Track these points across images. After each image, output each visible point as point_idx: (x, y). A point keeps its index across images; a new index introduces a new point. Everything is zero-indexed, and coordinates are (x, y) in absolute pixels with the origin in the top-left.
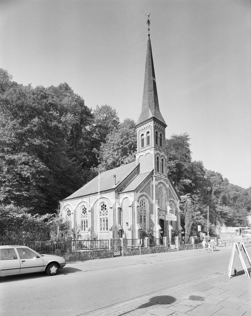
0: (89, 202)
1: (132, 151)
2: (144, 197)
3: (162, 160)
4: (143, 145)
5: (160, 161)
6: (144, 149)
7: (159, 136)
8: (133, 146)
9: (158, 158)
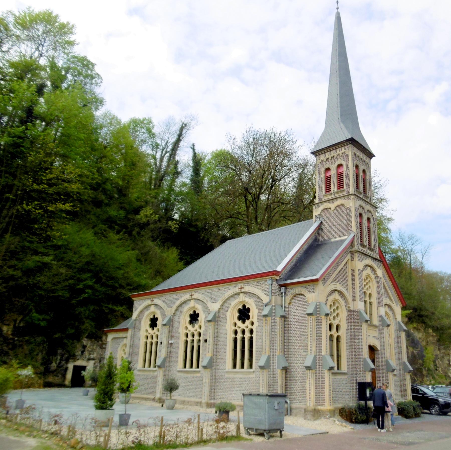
0: (209, 303)
1: (416, 347)
2: (336, 296)
3: (369, 219)
4: (328, 189)
5: (365, 222)
6: (330, 197)
7: (361, 173)
8: (44, 196)
9: (361, 215)
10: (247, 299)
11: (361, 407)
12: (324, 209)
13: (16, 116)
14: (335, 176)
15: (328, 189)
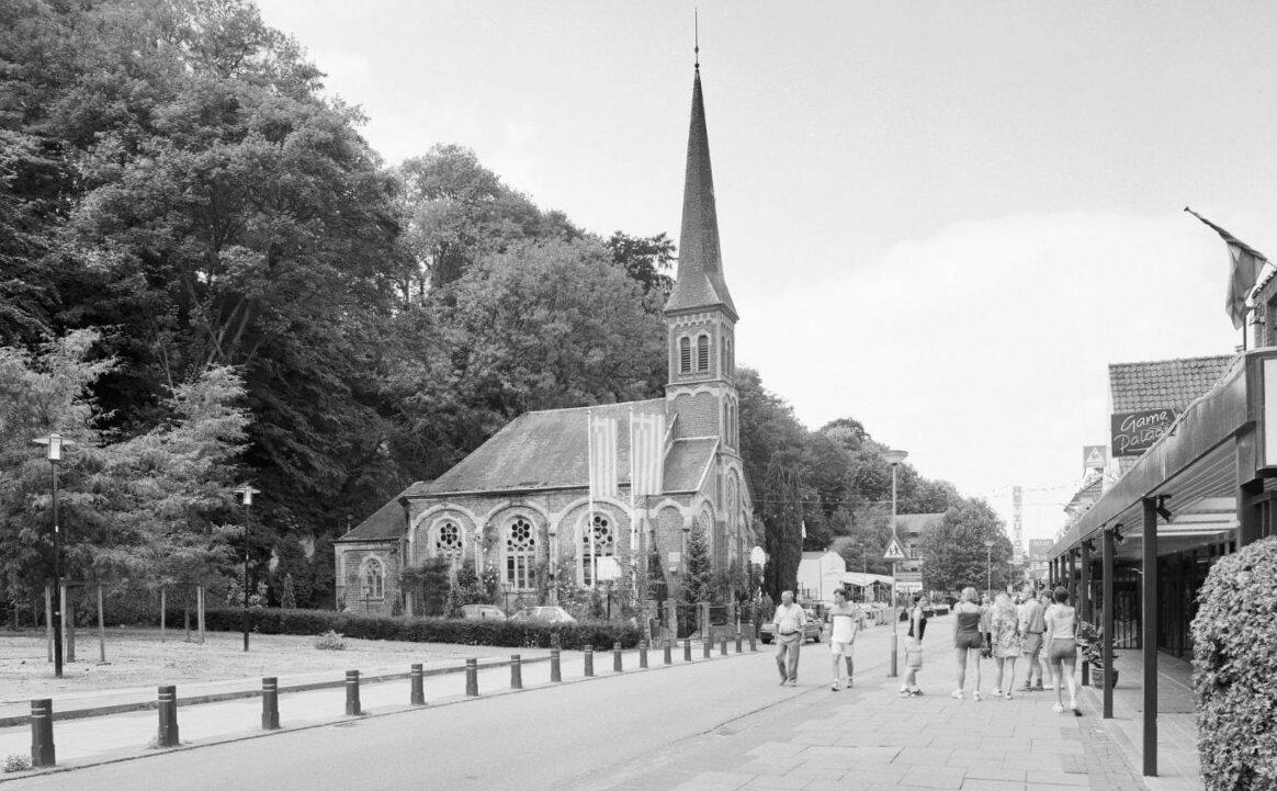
10: (453, 518)
11: (1070, 660)
12: (681, 395)
13: (196, 46)
14: (697, 349)
15: (686, 367)
